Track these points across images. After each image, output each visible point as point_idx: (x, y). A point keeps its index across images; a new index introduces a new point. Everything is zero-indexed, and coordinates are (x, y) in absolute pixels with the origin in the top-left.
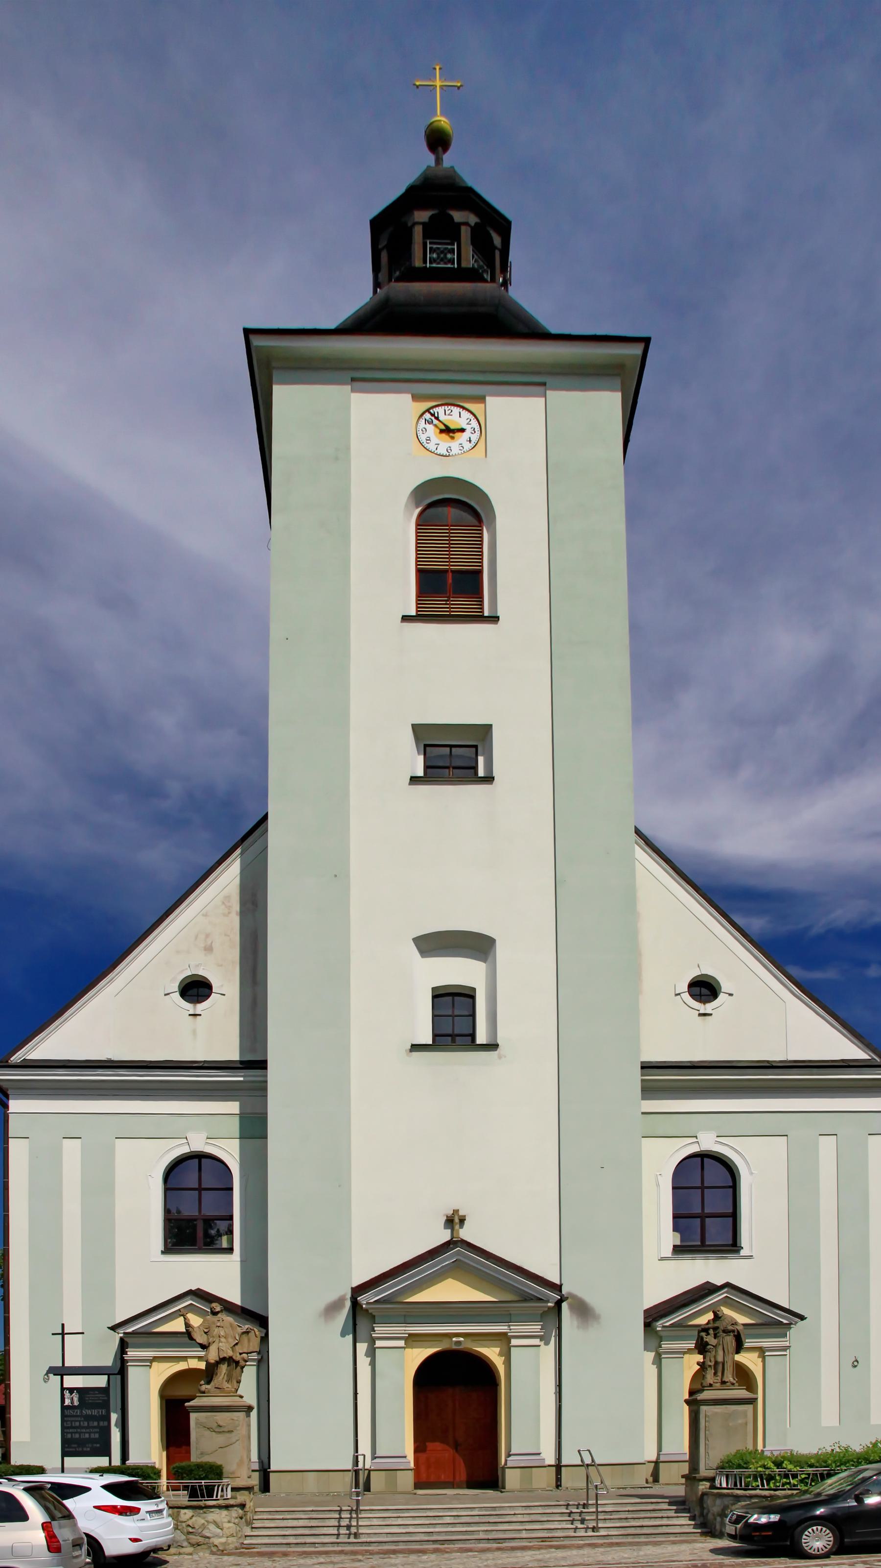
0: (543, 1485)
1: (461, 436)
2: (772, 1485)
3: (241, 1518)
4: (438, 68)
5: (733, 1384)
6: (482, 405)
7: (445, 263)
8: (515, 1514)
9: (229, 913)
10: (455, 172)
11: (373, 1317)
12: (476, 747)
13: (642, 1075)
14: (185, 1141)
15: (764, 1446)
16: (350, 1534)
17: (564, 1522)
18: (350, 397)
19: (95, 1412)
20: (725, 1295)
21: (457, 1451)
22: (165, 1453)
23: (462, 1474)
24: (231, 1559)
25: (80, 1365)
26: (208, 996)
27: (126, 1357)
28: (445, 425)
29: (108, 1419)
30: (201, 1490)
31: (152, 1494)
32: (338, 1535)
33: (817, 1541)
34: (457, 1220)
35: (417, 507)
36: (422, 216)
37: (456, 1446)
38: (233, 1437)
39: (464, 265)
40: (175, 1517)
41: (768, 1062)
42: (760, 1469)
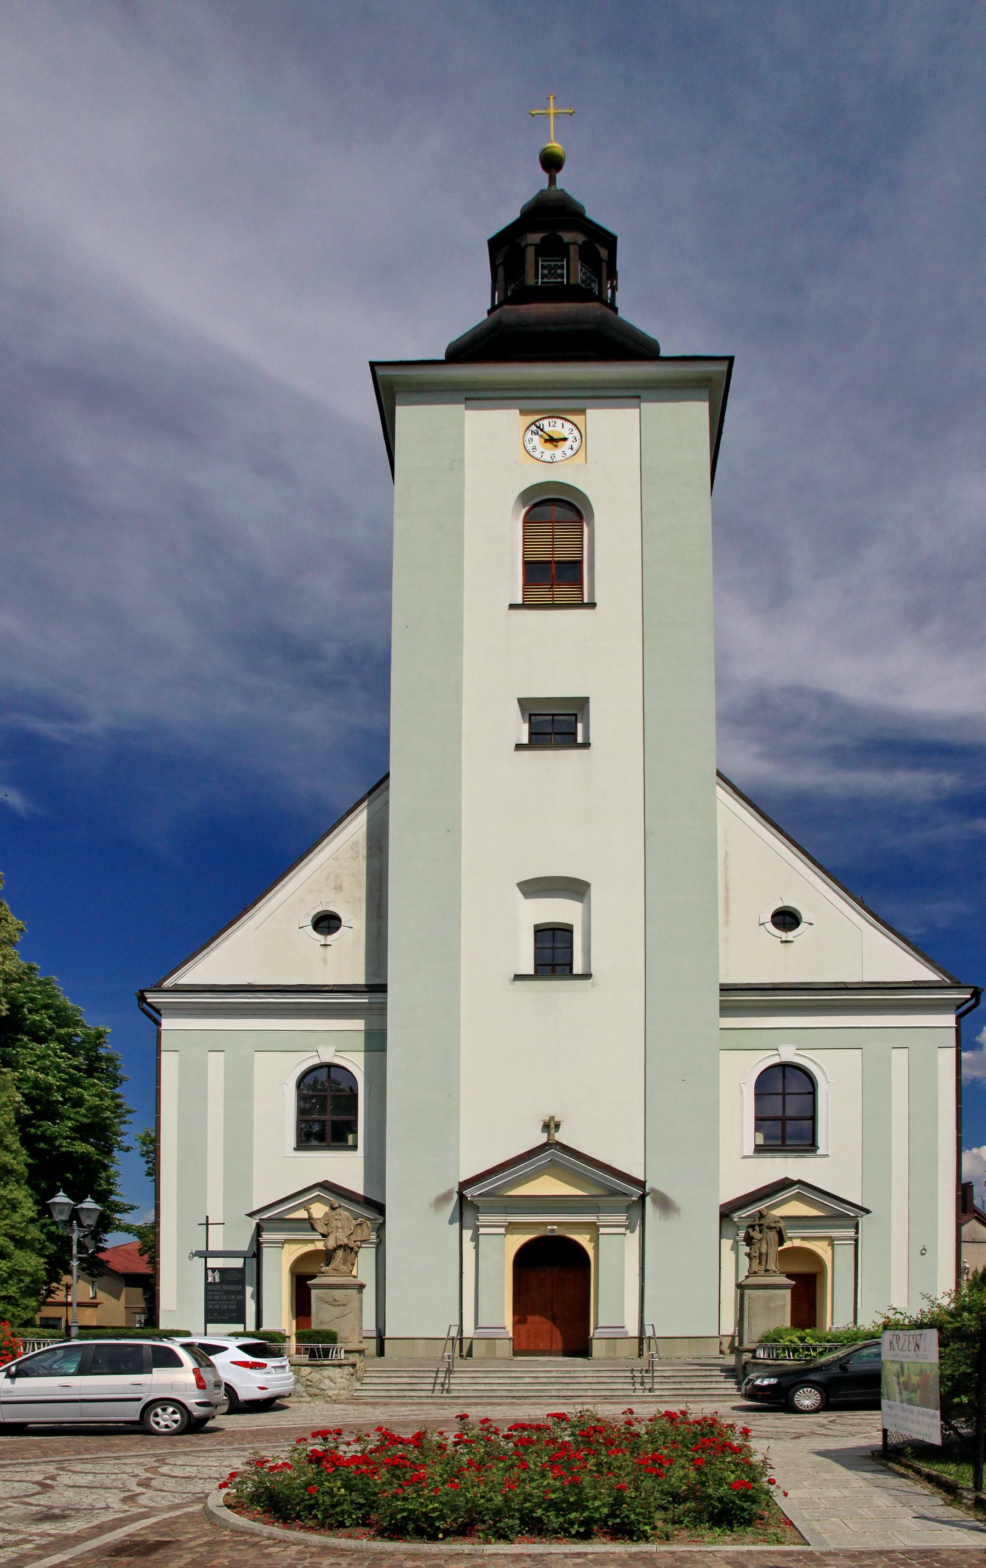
0: (626, 1354)
1: (564, 445)
2: (796, 1356)
3: (352, 1375)
4: (552, 97)
5: (775, 1272)
6: (582, 417)
7: (556, 278)
8: (585, 1377)
9: (357, 857)
12: (576, 715)
13: (720, 996)
14: (316, 1054)
15: (832, 1324)
16: (443, 1390)
17: (627, 1384)
18: (463, 416)
20: (797, 1190)
21: (554, 1323)
22: (294, 1322)
23: (559, 1345)
24: (341, 1406)
25: (222, 1250)
26: (337, 928)
27: (261, 1240)
28: (549, 436)
29: (243, 1293)
30: (319, 1352)
31: (277, 1354)
32: (433, 1390)
33: (807, 1400)
34: (552, 1125)
35: (524, 507)
36: (535, 238)
37: (554, 1319)
38: (347, 1309)
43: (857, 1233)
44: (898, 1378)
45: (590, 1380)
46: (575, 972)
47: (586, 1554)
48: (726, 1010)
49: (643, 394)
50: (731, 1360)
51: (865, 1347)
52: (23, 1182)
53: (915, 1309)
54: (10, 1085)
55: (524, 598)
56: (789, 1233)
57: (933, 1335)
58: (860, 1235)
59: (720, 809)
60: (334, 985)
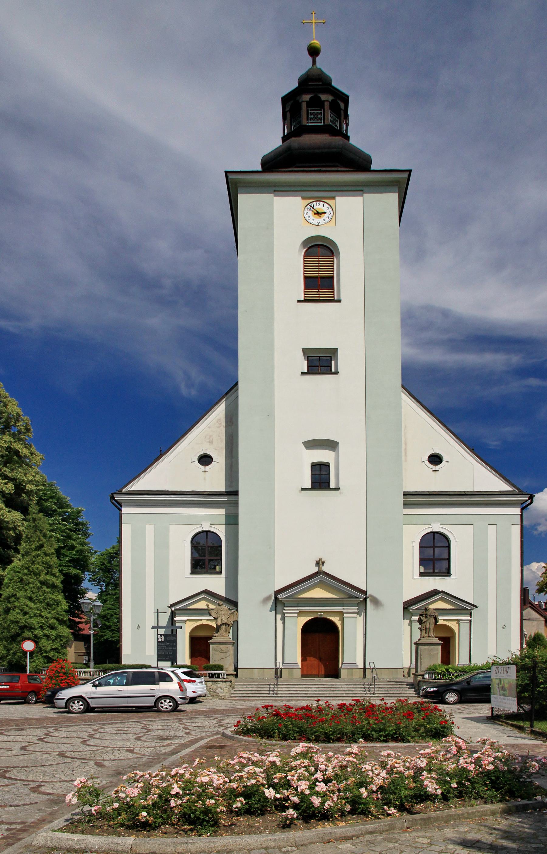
2: (444, 678)
4: (313, 13)
6: (334, 201)
7: (317, 120)
10: (322, 72)
11: (284, 604)
12: (331, 357)
13: (404, 498)
15: (459, 663)
19: (171, 644)
21: (320, 661)
23: (323, 672)
28: (317, 211)
30: (215, 675)
32: (269, 694)
34: (321, 563)
35: (304, 249)
36: (307, 97)
37: (320, 659)
38: (227, 654)
39: (326, 123)
40: (206, 684)
41: (464, 492)
42: (440, 672)
43: (471, 617)
44: (498, 685)
45: (344, 689)
46: (331, 487)
47: (389, 746)
48: (406, 505)
49: (365, 189)
50: (411, 680)
51: (478, 673)
52: (61, 591)
53: (505, 657)
54: (54, 543)
55: (304, 296)
56: (440, 617)
57: (514, 668)
58: (472, 619)
59: (403, 403)
60: (209, 491)
